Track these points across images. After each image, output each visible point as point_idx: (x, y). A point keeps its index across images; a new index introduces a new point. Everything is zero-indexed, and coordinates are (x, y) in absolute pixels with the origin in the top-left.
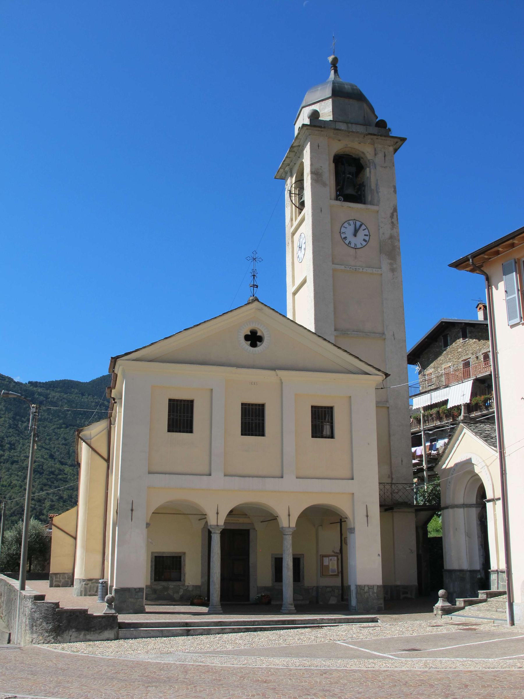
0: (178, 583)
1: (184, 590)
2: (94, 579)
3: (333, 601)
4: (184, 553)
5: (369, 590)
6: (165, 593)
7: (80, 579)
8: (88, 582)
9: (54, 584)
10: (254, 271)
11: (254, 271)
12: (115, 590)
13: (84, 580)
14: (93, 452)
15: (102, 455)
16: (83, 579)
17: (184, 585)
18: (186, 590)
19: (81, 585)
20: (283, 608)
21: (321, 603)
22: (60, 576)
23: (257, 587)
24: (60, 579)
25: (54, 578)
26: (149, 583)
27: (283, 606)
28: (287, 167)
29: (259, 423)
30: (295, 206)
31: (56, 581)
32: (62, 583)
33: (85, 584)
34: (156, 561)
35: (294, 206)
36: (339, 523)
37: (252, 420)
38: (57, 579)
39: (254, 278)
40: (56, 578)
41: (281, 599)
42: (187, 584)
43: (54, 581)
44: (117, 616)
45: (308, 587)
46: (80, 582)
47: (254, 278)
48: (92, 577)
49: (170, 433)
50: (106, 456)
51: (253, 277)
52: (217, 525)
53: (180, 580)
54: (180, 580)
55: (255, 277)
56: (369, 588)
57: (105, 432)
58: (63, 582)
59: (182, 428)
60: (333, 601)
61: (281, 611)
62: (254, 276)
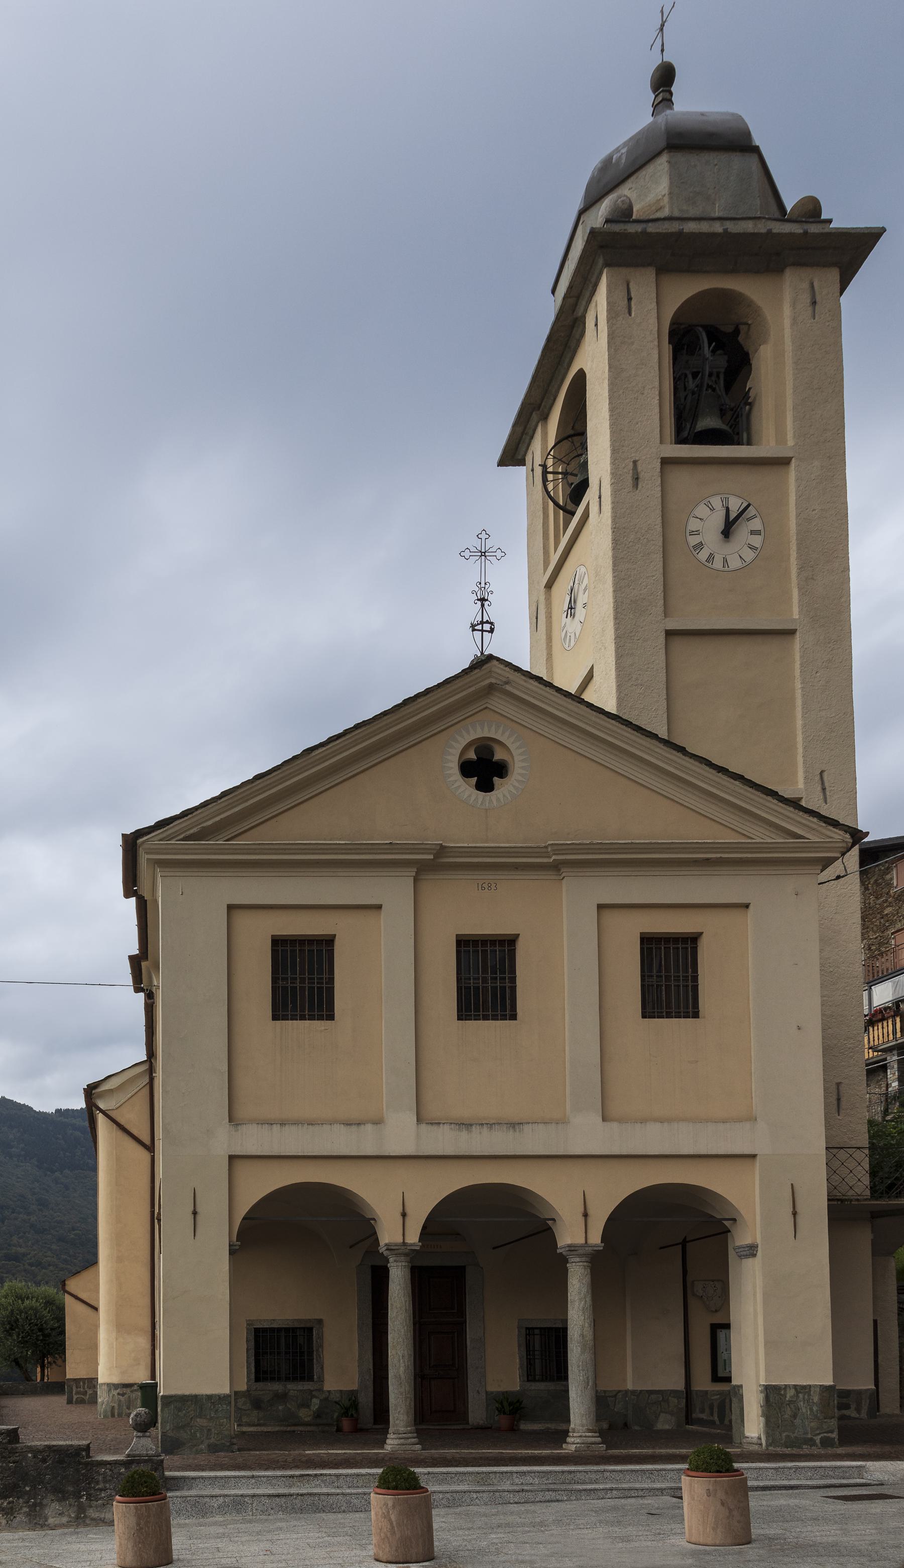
0: (307, 1386)
1: (320, 1400)
2: (135, 1384)
3: (665, 1423)
4: (320, 1322)
5: (798, 1396)
6: (280, 1408)
7: (108, 1384)
8: (125, 1390)
9: (75, 1397)
10: (483, 585)
11: (483, 585)
12: (162, 1396)
13: (116, 1386)
14: (120, 1133)
15: (135, 1132)
16: (114, 1385)
17: (320, 1390)
18: (326, 1399)
19: (111, 1395)
20: (569, 1440)
21: (637, 1428)
22: (84, 1383)
23: (487, 1392)
24: (84, 1388)
25: (74, 1388)
26: (243, 1387)
27: (571, 1434)
28: (534, 414)
29: (503, 989)
30: (556, 504)
31: (77, 1393)
32: (88, 1397)
33: (118, 1394)
34: (257, 1337)
35: (551, 504)
36: (680, 1246)
37: (485, 980)
38: (79, 1389)
39: (483, 605)
40: (77, 1387)
41: (568, 1421)
42: (326, 1388)
43: (74, 1392)
44: (162, 1461)
45: (605, 1392)
46: (110, 1390)
47: (483, 605)
48: (131, 1381)
49: (278, 1022)
50: (147, 1140)
51: (479, 603)
52: (404, 1244)
53: (310, 1378)
54: (310, 1378)
55: (486, 603)
56: (798, 1392)
57: (146, 1091)
58: (90, 1394)
59: (307, 1011)
60: (665, 1423)
61: (564, 1446)
62: (483, 600)
